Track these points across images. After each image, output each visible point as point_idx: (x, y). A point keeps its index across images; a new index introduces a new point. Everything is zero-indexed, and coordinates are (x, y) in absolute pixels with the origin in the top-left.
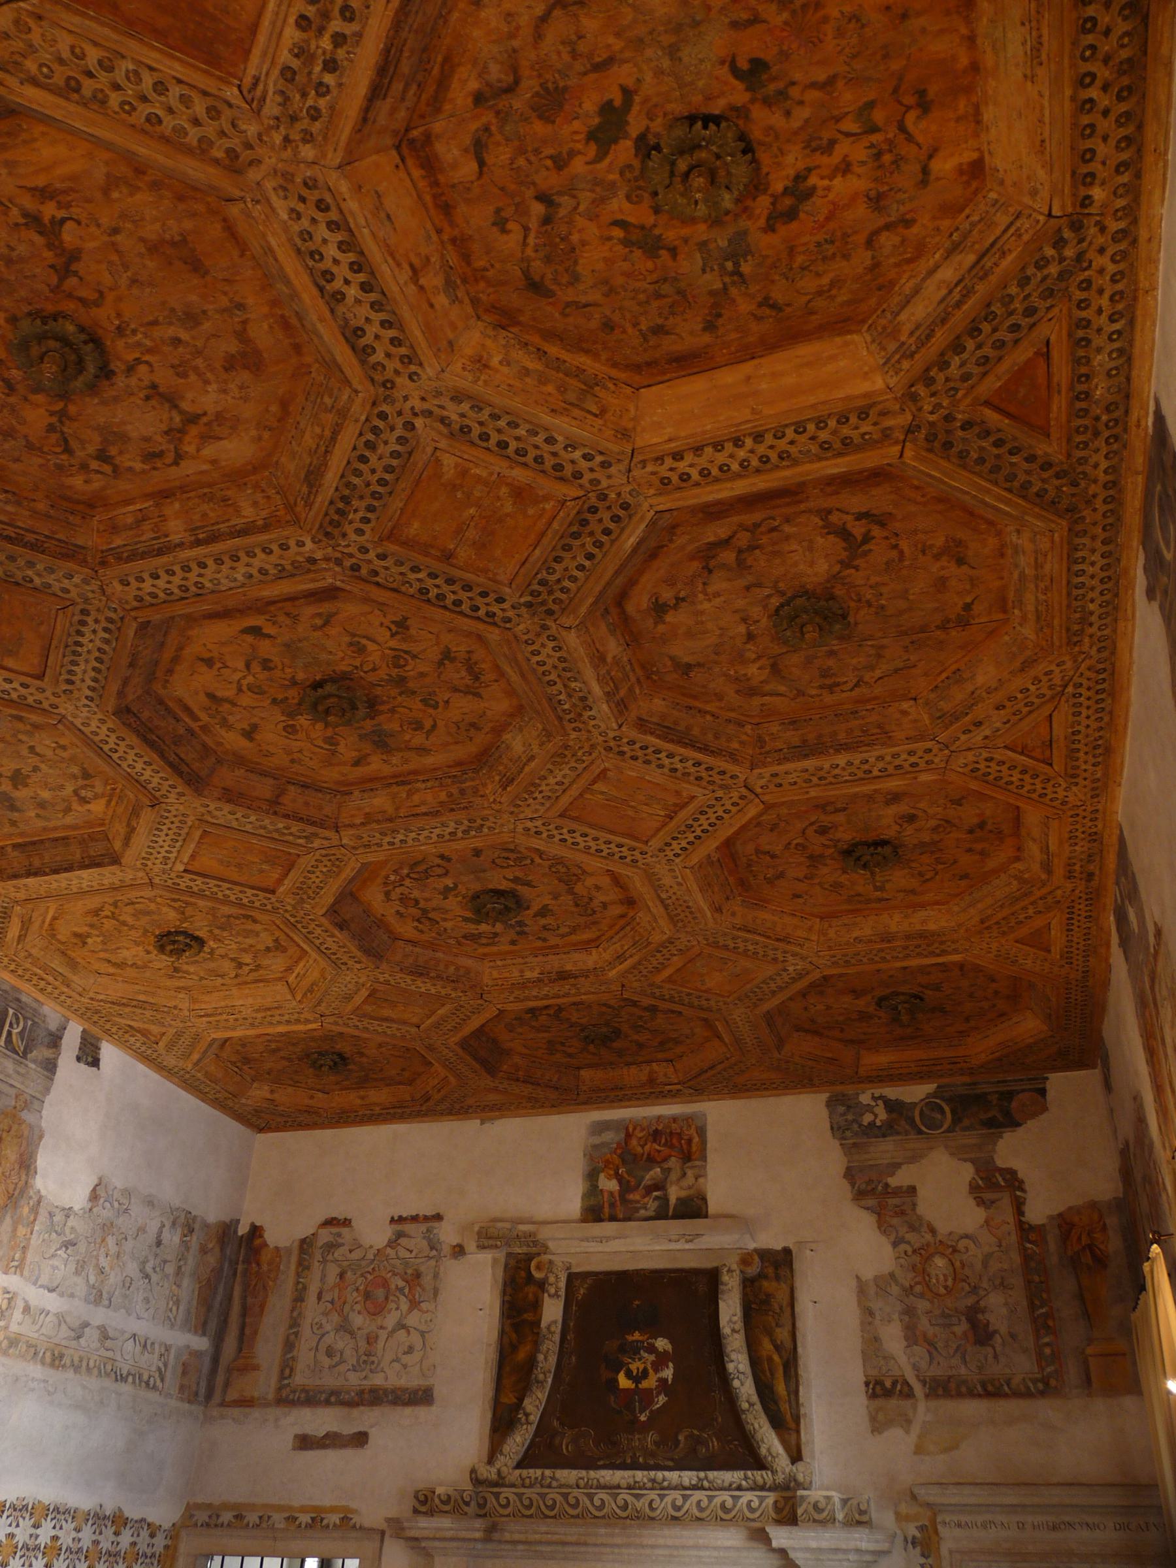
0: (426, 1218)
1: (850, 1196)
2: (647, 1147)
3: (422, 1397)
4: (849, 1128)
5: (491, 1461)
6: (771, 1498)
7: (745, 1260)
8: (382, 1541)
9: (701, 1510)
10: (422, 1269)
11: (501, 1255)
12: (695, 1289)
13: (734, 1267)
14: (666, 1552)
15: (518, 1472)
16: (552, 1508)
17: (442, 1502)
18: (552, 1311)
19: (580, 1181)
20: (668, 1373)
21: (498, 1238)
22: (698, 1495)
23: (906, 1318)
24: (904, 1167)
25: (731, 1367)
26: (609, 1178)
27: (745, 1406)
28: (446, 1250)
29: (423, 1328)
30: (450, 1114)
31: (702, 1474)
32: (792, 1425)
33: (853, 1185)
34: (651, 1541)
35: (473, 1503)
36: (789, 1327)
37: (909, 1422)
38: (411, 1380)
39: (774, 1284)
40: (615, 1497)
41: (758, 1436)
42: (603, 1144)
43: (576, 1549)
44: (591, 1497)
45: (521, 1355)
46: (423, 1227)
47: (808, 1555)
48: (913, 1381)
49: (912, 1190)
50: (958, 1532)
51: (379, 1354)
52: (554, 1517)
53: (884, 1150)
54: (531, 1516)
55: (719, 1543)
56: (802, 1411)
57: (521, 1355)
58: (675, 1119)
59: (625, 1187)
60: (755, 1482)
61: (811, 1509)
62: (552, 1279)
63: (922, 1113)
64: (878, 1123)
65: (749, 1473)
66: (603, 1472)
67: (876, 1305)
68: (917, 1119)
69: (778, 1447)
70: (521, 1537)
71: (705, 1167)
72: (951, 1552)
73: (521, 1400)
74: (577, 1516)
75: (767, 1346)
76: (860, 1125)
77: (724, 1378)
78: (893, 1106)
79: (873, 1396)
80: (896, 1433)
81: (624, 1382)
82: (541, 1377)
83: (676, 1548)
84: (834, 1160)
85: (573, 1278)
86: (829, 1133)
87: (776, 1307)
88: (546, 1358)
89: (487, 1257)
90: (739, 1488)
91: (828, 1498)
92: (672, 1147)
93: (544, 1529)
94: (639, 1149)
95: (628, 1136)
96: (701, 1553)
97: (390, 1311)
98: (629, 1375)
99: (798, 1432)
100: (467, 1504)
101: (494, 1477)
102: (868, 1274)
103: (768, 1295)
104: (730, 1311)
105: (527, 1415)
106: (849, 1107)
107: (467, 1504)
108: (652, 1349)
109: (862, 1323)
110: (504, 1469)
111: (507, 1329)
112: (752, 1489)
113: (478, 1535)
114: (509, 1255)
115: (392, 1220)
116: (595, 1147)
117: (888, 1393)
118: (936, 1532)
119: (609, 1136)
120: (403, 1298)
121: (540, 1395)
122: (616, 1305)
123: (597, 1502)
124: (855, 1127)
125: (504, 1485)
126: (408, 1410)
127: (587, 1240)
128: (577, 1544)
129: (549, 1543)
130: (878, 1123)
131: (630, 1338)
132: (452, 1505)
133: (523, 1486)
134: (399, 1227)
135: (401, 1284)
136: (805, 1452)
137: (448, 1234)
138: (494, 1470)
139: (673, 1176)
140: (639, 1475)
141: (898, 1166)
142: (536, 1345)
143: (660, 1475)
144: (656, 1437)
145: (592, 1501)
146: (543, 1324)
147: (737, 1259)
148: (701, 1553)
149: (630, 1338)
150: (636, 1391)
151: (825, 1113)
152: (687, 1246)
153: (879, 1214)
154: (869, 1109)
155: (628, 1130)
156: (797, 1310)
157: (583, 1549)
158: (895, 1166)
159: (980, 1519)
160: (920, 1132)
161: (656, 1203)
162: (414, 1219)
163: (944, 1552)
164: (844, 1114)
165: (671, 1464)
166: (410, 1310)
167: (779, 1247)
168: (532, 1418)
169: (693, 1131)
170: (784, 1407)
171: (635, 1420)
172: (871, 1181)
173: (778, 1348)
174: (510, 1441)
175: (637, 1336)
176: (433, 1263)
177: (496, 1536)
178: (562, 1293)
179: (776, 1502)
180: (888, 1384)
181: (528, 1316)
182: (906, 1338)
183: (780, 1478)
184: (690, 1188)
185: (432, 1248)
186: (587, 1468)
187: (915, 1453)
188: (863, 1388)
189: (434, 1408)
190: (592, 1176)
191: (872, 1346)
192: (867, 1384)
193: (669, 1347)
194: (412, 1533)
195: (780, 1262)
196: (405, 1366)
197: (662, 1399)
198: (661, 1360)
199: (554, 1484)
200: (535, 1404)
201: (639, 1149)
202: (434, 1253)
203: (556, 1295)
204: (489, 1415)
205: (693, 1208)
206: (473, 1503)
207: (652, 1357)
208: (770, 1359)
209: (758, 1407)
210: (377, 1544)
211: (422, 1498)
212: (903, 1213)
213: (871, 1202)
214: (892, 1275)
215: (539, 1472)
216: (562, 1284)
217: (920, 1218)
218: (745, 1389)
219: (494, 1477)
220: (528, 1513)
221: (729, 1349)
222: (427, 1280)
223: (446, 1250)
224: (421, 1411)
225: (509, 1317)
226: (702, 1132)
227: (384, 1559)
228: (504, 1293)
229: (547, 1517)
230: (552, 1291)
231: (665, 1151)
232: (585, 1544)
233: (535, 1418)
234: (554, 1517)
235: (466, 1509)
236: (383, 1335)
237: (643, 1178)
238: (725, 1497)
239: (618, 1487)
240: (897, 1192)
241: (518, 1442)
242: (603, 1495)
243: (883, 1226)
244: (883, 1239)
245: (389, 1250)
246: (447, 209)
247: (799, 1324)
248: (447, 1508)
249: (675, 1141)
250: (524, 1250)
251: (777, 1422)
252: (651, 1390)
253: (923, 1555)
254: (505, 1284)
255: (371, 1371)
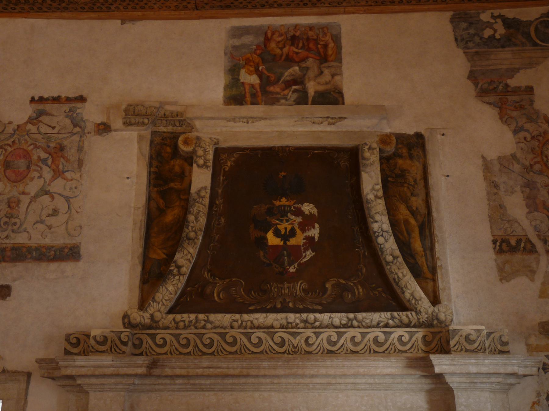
0: (68, 100)
1: (473, 93)
2: (286, 50)
3: (70, 253)
4: (471, 38)
5: (142, 306)
6: (420, 333)
7: (384, 140)
8: (28, 382)
9: (356, 344)
10: (65, 143)
11: (147, 133)
12: (335, 167)
13: (375, 145)
14: (324, 381)
15: (171, 316)
16: (210, 346)
17: (98, 343)
18: (201, 179)
19: (222, 74)
20: (315, 232)
21: (146, 115)
22: (351, 332)
23: (528, 190)
24: (522, 71)
25: (375, 227)
26: (250, 74)
27: (389, 258)
28: (90, 127)
29: (67, 193)
30: (91, 10)
31: (351, 315)
32: (429, 275)
33: (476, 85)
34: (313, 371)
35: (130, 344)
36: (422, 196)
37: (533, 272)
38: (57, 239)
39: (408, 162)
40: (272, 335)
41: (402, 283)
42: (243, 46)
43: (235, 381)
44: (248, 336)
45: (170, 217)
46: (66, 107)
47: (463, 379)
48: (535, 240)
49: (530, 90)
51: (22, 216)
52: (212, 354)
53: (504, 58)
54: (189, 354)
55: (379, 371)
56: (439, 263)
57: (170, 217)
58: (311, 28)
59: (265, 82)
60: (401, 321)
61: (463, 339)
62: (200, 152)
63: (536, 29)
64: (497, 36)
65: (395, 314)
66: (257, 315)
67: (501, 179)
68: (533, 34)
69: (419, 293)
70: (183, 372)
71: (340, 67)
73: (171, 256)
74: (236, 353)
75: (403, 212)
76: (481, 38)
77: (368, 238)
78: (508, 23)
79: (500, 252)
80: (522, 281)
81: (272, 239)
82: (192, 235)
83: (335, 376)
84: (459, 64)
85: (220, 153)
86: (453, 44)
87: (411, 180)
88: (196, 219)
89: (132, 134)
90: (387, 326)
91: (478, 331)
92: (309, 50)
93: (206, 364)
94: (278, 51)
95: (267, 40)
96: (358, 381)
97: (32, 179)
98: (277, 233)
99: (434, 280)
100: (125, 344)
101: (148, 321)
102: (492, 155)
103: (403, 171)
104: (371, 181)
105: (179, 267)
106: (471, 24)
107: (125, 344)
108: (298, 213)
109: (488, 194)
110: (158, 315)
111: (154, 195)
112: (398, 327)
113: (140, 371)
114: (154, 133)
115: (33, 100)
116: (234, 47)
117: (513, 250)
119: (248, 39)
120: (46, 169)
121: (191, 250)
122: (258, 176)
123: (254, 340)
124: (477, 39)
125: (157, 328)
126: (53, 266)
127: (234, 120)
128: (238, 376)
129: (209, 376)
130: (497, 36)
131: (277, 203)
132: (107, 345)
133: (177, 328)
134: (41, 107)
135: (43, 155)
136: (443, 296)
137: (91, 114)
138: (147, 315)
139: (311, 74)
140: (292, 317)
141: (517, 70)
142: (186, 210)
143: (311, 317)
144: (305, 285)
145: (249, 340)
146: (193, 190)
147: (377, 139)
148: (358, 381)
149: (277, 203)
150: (285, 247)
151: (449, 27)
152: (329, 129)
153: (500, 108)
154: (489, 25)
155: (268, 36)
156: (431, 182)
157: (242, 381)
158: (513, 72)
160: (535, 44)
161: (295, 95)
162: (56, 100)
164: (467, 29)
165: (320, 308)
166: (54, 178)
167: (412, 133)
168: (184, 270)
169: (328, 38)
170: (422, 261)
171: (284, 272)
172: (492, 82)
173: (414, 213)
174: (162, 290)
175: (284, 201)
176: (76, 138)
177: (157, 371)
178: (210, 164)
179: (424, 337)
180: (513, 242)
181: (175, 185)
182: (528, 206)
183: (424, 317)
184: (327, 83)
185: (75, 126)
186: (240, 312)
187: (540, 297)
188: (491, 245)
189: (81, 264)
190: (233, 71)
191: (497, 212)
192: (494, 242)
193: (315, 211)
194: (68, 372)
195: (414, 145)
196: (50, 227)
197: (309, 254)
198: (307, 222)
199: (209, 326)
200: (186, 258)
201: (278, 51)
202: (78, 129)
203: (205, 165)
204: (139, 269)
205: (332, 97)
206: (130, 344)
207: (299, 219)
208: (407, 222)
209: (401, 259)
210: (23, 386)
211: (75, 341)
212: (522, 107)
213: (492, 99)
214: (514, 156)
215: (193, 316)
216: (210, 157)
217: (537, 112)
218: (388, 245)
219: (148, 321)
220: (187, 351)
221: (373, 212)
222: (71, 153)
223: (90, 127)
224: (68, 267)
225: (155, 186)
226: (337, 39)
227: (30, 399)
228: (150, 165)
229: (204, 354)
230: (201, 162)
231: (303, 53)
232: (247, 376)
233: (186, 270)
234: (212, 354)
235: (124, 348)
236: (25, 200)
237: (282, 74)
238: (378, 333)
239: (272, 327)
240: (517, 91)
241: (170, 290)
242: (260, 334)
243: (504, 118)
244: (505, 128)
245: (29, 126)
247: (433, 193)
248: (103, 348)
249: (311, 45)
250: (170, 129)
251: (417, 273)
252: (299, 246)
254: (151, 157)
255: (13, 231)
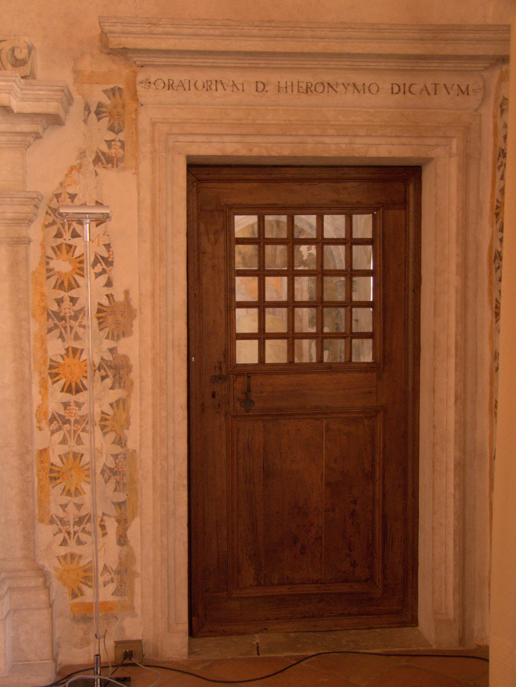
50: (167, 96)
72: (153, 124)
118: (135, 97)
159: (201, 77)
163: (144, 122)
246: (484, 87)
253: (111, 129)
